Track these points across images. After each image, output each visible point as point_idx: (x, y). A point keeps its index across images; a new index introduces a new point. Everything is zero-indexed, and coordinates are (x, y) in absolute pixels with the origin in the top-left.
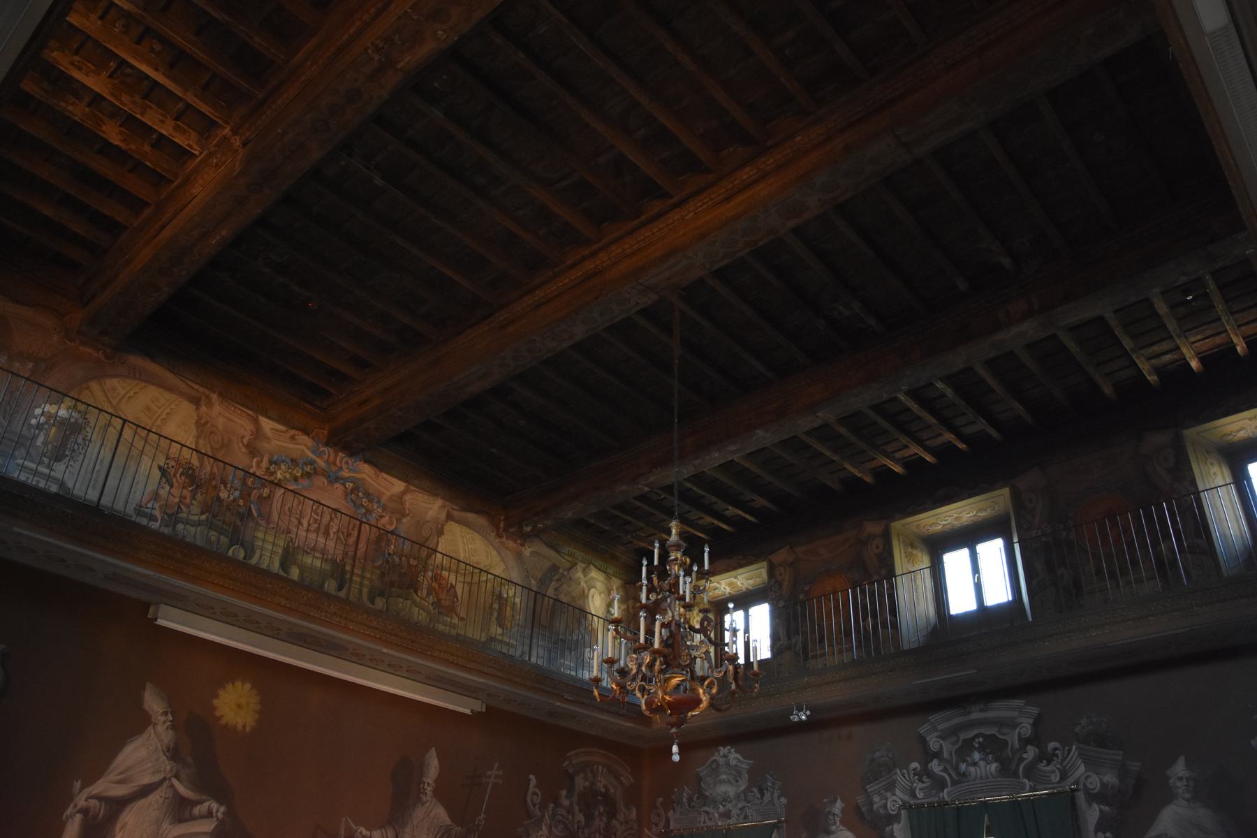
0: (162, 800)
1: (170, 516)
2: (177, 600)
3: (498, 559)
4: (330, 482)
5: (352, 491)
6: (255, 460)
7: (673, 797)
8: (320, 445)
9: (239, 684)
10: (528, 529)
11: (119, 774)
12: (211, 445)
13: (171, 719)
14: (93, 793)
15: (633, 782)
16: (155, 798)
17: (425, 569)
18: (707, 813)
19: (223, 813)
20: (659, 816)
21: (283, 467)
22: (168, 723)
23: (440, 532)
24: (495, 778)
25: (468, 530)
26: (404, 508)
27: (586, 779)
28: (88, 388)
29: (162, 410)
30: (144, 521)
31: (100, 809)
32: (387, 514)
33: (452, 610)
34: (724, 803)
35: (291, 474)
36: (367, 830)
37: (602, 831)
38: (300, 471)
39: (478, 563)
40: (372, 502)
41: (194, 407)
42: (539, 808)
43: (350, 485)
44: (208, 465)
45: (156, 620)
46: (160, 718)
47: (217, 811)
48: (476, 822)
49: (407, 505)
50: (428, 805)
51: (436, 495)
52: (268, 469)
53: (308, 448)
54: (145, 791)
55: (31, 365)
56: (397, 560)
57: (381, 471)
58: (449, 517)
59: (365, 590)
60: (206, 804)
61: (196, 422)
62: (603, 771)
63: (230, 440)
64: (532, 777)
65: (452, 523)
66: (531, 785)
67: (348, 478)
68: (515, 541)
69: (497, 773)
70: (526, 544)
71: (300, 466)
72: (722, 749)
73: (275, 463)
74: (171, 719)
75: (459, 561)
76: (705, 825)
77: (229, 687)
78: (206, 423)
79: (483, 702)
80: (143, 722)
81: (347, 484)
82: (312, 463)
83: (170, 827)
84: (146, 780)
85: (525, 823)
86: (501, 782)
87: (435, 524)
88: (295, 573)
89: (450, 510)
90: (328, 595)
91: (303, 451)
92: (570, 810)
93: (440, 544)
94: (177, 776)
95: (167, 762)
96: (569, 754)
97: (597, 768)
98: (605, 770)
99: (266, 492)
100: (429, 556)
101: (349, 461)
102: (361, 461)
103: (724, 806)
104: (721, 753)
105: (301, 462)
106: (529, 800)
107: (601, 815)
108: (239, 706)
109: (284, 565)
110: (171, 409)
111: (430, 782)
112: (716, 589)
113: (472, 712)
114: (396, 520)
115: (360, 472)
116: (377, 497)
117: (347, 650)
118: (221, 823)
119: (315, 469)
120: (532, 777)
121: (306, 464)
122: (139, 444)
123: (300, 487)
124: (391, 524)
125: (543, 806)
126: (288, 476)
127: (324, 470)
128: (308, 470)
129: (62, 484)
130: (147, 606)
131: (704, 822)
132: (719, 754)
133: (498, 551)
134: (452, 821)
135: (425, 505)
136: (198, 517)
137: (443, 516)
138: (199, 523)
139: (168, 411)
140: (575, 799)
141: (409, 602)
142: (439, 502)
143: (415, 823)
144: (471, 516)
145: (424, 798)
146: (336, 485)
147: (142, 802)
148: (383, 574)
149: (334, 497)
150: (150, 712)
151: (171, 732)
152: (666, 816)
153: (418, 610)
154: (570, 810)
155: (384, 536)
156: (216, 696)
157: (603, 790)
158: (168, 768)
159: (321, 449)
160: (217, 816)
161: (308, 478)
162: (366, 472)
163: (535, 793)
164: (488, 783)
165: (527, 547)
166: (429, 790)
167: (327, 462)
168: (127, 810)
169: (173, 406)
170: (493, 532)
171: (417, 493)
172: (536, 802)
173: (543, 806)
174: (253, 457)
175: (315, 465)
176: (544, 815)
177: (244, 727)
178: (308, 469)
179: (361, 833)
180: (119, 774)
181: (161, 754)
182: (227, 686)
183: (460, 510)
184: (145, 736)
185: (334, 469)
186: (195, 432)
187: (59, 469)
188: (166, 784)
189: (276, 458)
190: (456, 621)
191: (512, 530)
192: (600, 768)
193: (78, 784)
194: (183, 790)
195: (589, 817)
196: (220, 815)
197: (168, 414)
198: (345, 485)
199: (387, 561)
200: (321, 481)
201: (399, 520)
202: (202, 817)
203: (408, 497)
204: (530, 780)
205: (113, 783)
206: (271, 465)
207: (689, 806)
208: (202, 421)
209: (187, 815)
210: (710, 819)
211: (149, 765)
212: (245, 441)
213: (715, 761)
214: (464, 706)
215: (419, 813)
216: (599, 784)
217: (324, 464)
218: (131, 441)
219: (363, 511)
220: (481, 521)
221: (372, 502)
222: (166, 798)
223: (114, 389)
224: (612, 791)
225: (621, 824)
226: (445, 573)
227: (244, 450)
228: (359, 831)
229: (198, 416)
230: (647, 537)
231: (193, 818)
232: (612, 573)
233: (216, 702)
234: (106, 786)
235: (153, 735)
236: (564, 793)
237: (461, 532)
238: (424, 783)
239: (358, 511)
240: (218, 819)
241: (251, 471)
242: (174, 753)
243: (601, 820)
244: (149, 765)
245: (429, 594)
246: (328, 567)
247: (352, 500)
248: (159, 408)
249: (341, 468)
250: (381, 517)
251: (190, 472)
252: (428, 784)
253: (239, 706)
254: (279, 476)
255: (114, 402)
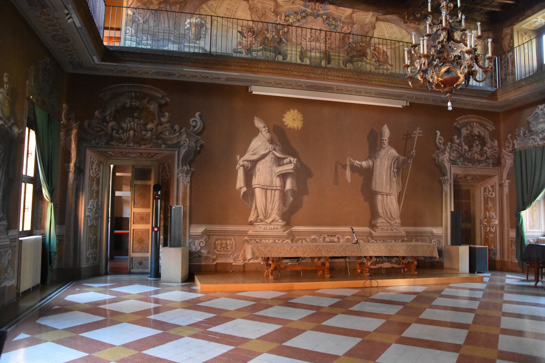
0: (270, 159)
1: (248, 50)
2: (256, 82)
3: (407, 34)
4: (315, 18)
5: (326, 19)
6: (278, 17)
7: (516, 133)
8: (307, 2)
9: (292, 111)
10: (419, 16)
11: (252, 152)
12: (258, 16)
13: (267, 129)
14: (245, 159)
15: (494, 128)
16: (268, 158)
17: (369, 46)
18: (533, 139)
19: (296, 161)
20: (510, 143)
21: (291, 16)
22: (266, 131)
23: (374, 28)
24: (418, 134)
25: (388, 23)
26: (354, 21)
27: (467, 130)
28: (202, 8)
29: (233, 7)
30: (238, 55)
31: (248, 165)
32: (345, 25)
33: (386, 62)
34: (542, 133)
35: (296, 19)
36: (359, 161)
37: (479, 153)
38: (300, 17)
39: (396, 38)
40: (337, 22)
41: (246, 2)
42: (443, 145)
43: (325, 17)
44: (260, 25)
45: (252, 92)
46: (263, 129)
47: (293, 161)
48: (411, 154)
49: (355, 19)
50: (386, 149)
51: (369, 11)
52: (285, 19)
53: (302, 6)
54: (263, 157)
55: (178, 6)
56: (354, 45)
57: (338, 6)
58: (377, 20)
59: (341, 62)
60: (288, 159)
61: (249, 9)
62: (476, 125)
63: (265, 12)
64: (438, 132)
65: (379, 22)
66: (438, 135)
67: (323, 14)
68: (415, 23)
69: (420, 131)
70: (421, 24)
71: (299, 14)
72: (540, 106)
73: (288, 16)
74: (267, 129)
75: (387, 40)
76: (533, 145)
77: (288, 113)
78: (253, 7)
79: (407, 101)
80: (256, 132)
81: (323, 16)
82: (305, 11)
83: (276, 168)
84: (263, 152)
85: (436, 152)
86: (422, 135)
87: (371, 25)
88: (307, 62)
89: (378, 16)
90: (322, 68)
91: (299, 7)
92: (460, 145)
93: (375, 33)
94: (274, 150)
95: (269, 145)
96: (456, 119)
97: (473, 124)
98: (478, 124)
99: (286, 30)
100: (370, 40)
101: (322, 6)
102: (328, 4)
103: (542, 135)
104: (540, 108)
105: (299, 13)
106: (437, 141)
107: (477, 145)
108: (294, 120)
109: (301, 59)
110: (237, 6)
111: (386, 139)
112: (535, 22)
113: (402, 106)
114: (351, 27)
115: (328, 10)
116: (339, 19)
117: (334, 89)
118: (296, 165)
119: (307, 14)
120: (438, 132)
121: (302, 13)
122: (230, 25)
123: (301, 23)
124: (348, 29)
125: (445, 144)
126: (295, 20)
127: (311, 13)
128: (304, 15)
129: (203, 49)
130: (247, 87)
131: (532, 144)
132: (539, 109)
133: (406, 30)
134: (399, 154)
135: (364, 17)
136: (256, 48)
137: (374, 19)
138: (261, 50)
139: (236, 7)
140: (462, 138)
141: (364, 63)
142: (371, 13)
143: (381, 157)
144: (389, 17)
145: (384, 146)
146: (318, 18)
147: (263, 161)
148: (348, 53)
149: (318, 24)
150: (259, 128)
151: (268, 134)
152: (513, 142)
153: (368, 65)
154: (460, 145)
155: (346, 35)
156: (284, 117)
157: (477, 134)
158: (270, 147)
159: (307, 4)
160: (294, 163)
161: (304, 18)
162: (331, 9)
163: (440, 139)
164: (415, 136)
165: (422, 25)
166: (386, 143)
167: (312, 9)
168: (259, 163)
169: (238, 4)
170: (402, 21)
171: (358, 12)
172: (441, 142)
173: (445, 144)
174: (277, 16)
175: (306, 12)
176: (446, 148)
177: (298, 127)
178: (303, 14)
179: (357, 163)
180: (252, 152)
181: (267, 142)
182: (287, 113)
183: (383, 15)
184: (258, 136)
185: (315, 11)
186: (249, 13)
187: (202, 43)
188: (271, 153)
189: (287, 14)
190: (389, 67)
191: (411, 18)
192: (475, 124)
193: (238, 157)
194: (278, 155)
195: (471, 147)
196: (295, 162)
197: (236, 8)
198: (322, 17)
199: (350, 47)
200: (310, 18)
201: (352, 27)
202: (287, 163)
203: (354, 15)
204: (437, 133)
205: (251, 155)
206: (286, 17)
207: (524, 137)
208: (252, 7)
209: (282, 163)
210: (535, 142)
211: (263, 147)
212: (272, 10)
213: (537, 113)
214: (398, 104)
215: (383, 152)
216: (475, 131)
217: (310, 10)
218: (227, 25)
219: (333, 27)
220: (395, 17)
221: (337, 22)
222: (272, 158)
223: (212, 5)
224: (483, 134)
225: (489, 148)
226: (381, 46)
227: (272, 14)
228: (356, 162)
229: (249, 5)
230: (490, 4)
231: (284, 164)
232: (473, 28)
233: (284, 120)
234: (249, 156)
235: (262, 136)
236: (456, 137)
237: (385, 25)
238: (383, 140)
239: (331, 27)
240: (294, 164)
241: (278, 22)
242: (271, 141)
243: (478, 148)
244: (263, 147)
245: (373, 57)
246: (322, 55)
247: (327, 23)
248: (232, 7)
249: (319, 10)
250: (343, 27)
251: (252, 30)
252: (385, 140)
253: (294, 120)
254: (291, 21)
255: (213, 10)
